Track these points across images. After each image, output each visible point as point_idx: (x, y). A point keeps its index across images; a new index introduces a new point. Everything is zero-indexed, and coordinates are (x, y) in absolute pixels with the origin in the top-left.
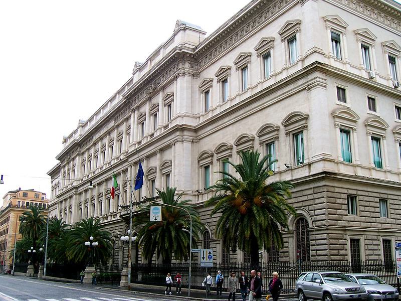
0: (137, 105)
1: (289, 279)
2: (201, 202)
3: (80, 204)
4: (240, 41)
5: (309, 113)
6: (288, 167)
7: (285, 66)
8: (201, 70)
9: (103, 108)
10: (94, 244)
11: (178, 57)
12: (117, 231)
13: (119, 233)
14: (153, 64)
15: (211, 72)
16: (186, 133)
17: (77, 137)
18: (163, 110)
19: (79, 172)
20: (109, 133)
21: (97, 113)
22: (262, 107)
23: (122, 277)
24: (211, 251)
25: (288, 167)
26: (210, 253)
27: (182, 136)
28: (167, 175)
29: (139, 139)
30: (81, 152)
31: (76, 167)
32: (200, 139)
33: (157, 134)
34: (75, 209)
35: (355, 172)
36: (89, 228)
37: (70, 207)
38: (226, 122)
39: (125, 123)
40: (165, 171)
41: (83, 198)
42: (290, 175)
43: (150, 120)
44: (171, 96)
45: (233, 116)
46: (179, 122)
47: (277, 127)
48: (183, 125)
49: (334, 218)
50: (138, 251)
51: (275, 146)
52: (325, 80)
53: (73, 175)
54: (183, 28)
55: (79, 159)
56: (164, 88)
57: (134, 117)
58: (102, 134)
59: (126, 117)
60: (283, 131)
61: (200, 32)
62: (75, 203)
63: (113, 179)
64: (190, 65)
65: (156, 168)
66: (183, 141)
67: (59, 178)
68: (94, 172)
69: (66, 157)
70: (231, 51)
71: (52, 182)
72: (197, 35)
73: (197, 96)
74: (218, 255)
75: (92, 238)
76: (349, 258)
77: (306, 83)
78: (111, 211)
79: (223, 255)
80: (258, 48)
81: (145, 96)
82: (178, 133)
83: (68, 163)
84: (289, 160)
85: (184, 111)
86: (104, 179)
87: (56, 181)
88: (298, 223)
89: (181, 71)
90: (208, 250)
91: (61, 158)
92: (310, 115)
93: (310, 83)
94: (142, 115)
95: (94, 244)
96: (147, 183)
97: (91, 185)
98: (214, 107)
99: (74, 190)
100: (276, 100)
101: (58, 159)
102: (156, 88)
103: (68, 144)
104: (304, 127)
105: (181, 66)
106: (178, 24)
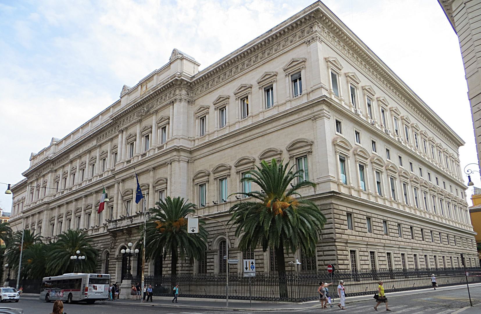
0: (125, 126)
2: (207, 214)
3: (52, 219)
5: (313, 140)
6: (215, 203)
7: (289, 98)
8: (196, 97)
9: (82, 128)
10: (80, 257)
11: (176, 83)
12: (99, 245)
13: (102, 247)
15: (208, 100)
16: (182, 154)
17: (50, 154)
19: (50, 188)
20: (89, 151)
22: (214, 151)
24: (254, 261)
25: (215, 203)
26: (252, 263)
27: (179, 156)
29: (128, 158)
30: (55, 169)
34: (46, 224)
35: (350, 192)
37: (40, 222)
38: (224, 146)
39: (69, 165)
41: (56, 213)
42: (216, 209)
43: (99, 162)
45: (232, 140)
46: (177, 143)
47: (281, 151)
48: (180, 146)
49: (339, 232)
51: (307, 162)
52: (329, 112)
53: (63, 183)
54: (177, 57)
55: (51, 176)
56: (157, 112)
57: (122, 138)
58: (81, 152)
59: (111, 137)
60: (233, 171)
61: (195, 63)
62: (46, 218)
64: (186, 93)
65: (92, 205)
66: (179, 161)
67: (26, 193)
68: (36, 203)
70: (230, 82)
72: (192, 65)
73: (192, 121)
74: (215, 265)
75: (78, 252)
76: (350, 267)
77: (311, 114)
78: (92, 224)
79: (220, 265)
80: (260, 81)
81: (136, 118)
82: (175, 153)
83: (37, 180)
84: (216, 198)
85: (180, 133)
86: (84, 195)
87: (20, 197)
88: (221, 244)
89: (178, 97)
90: (251, 261)
91: (27, 175)
92: (315, 142)
93: (316, 114)
95: (80, 257)
96: (154, 194)
98: (210, 132)
100: (279, 128)
101: (24, 176)
102: (148, 111)
103: (36, 161)
104: (309, 152)
105: (177, 92)
106: (174, 52)
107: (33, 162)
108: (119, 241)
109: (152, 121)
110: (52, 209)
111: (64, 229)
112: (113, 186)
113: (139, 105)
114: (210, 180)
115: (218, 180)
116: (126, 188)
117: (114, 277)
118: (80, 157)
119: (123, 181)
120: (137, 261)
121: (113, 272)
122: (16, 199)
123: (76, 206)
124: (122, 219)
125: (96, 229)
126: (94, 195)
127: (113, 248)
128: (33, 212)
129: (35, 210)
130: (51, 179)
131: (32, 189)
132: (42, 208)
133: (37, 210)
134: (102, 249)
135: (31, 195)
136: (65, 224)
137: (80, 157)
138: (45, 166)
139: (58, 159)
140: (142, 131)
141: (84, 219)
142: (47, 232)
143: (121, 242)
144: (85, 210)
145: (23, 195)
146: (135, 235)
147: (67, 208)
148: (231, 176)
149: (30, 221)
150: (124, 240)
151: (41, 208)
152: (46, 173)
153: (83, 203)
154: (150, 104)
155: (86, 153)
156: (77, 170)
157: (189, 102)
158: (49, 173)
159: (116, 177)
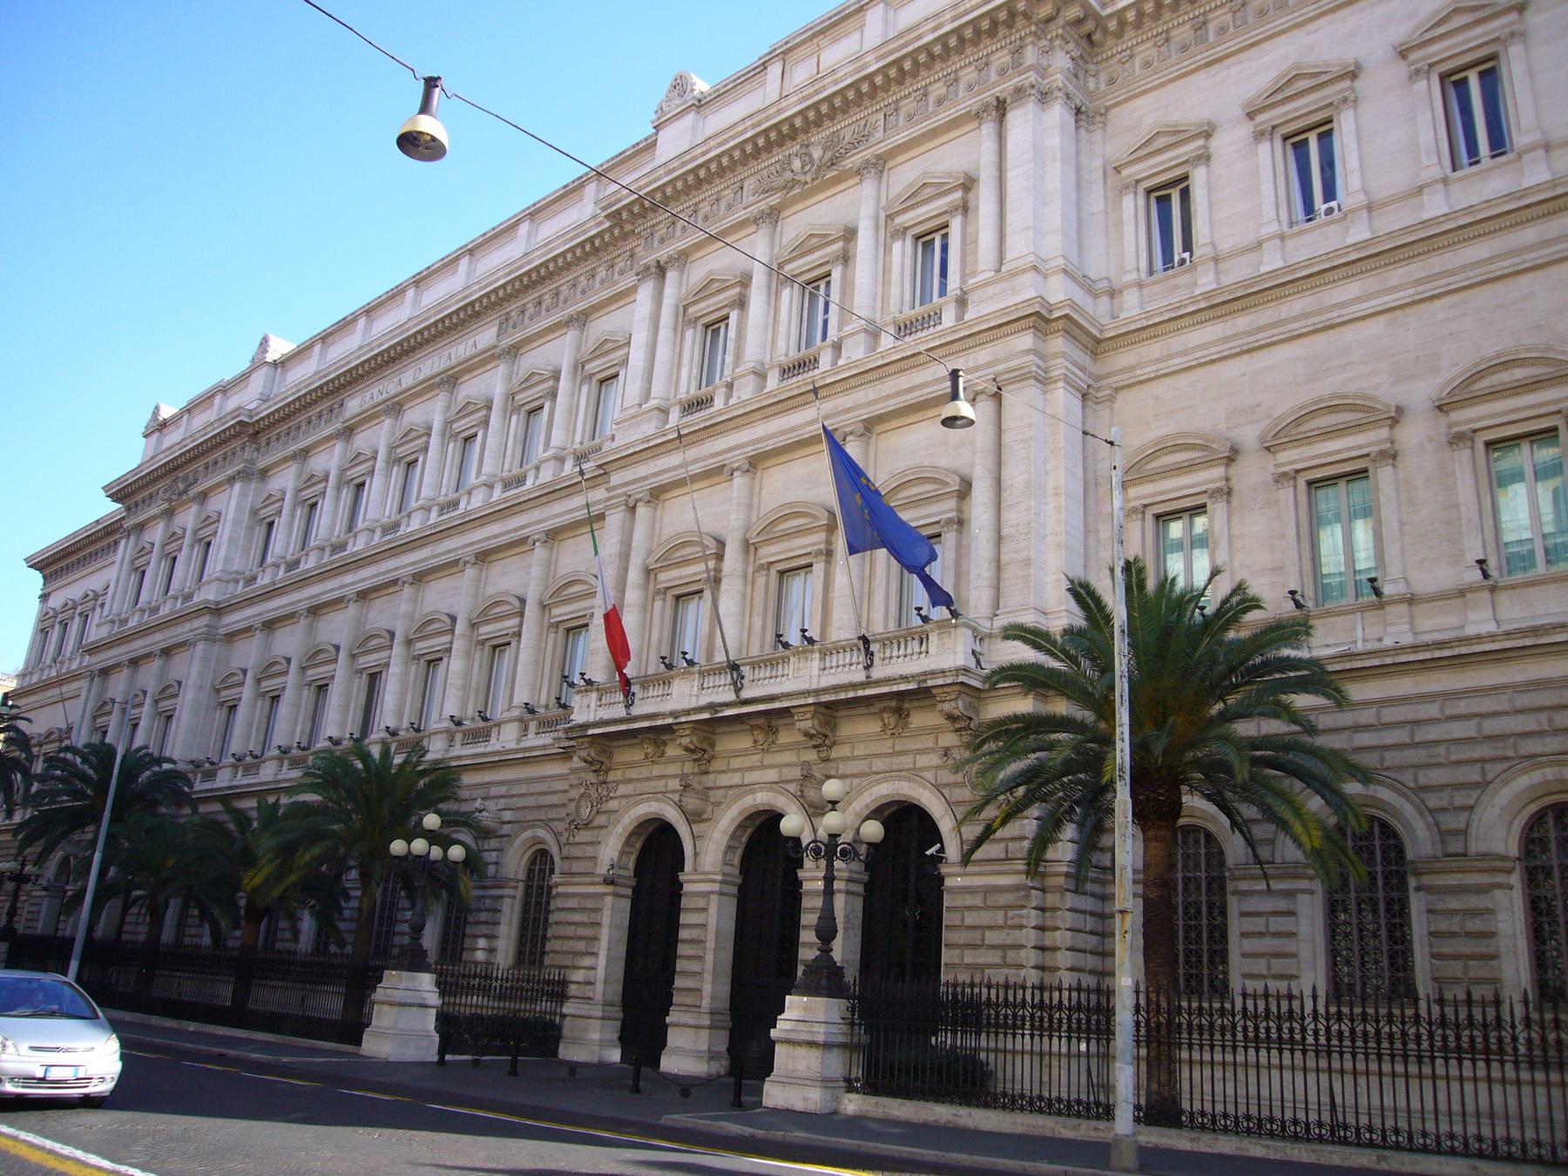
0: (681, 245)
4: (1282, 22)
14: (802, 73)
17: (248, 400)
21: (331, 334)
23: (778, 1048)
28: (320, 687)
30: (261, 465)
32: (1117, 390)
33: (309, 563)
37: (169, 691)
40: (268, 685)
44: (619, 347)
45: (1416, 269)
55: (243, 495)
56: (879, 165)
63: (540, 551)
67: (108, 575)
74: (1305, 954)
78: (236, 746)
83: (169, 513)
88: (533, 862)
91: (122, 492)
99: (205, 620)
103: (173, 437)
107: (159, 442)
108: (622, 789)
112: (595, 520)
113: (782, 135)
114: (1234, 483)
115: (1301, 484)
116: (490, 590)
122: (56, 602)
123: (549, 565)
126: (407, 590)
127: (587, 826)
128: (138, 646)
130: (239, 507)
132: (182, 631)
133: (159, 639)
134: (506, 829)
135: (134, 578)
136: (297, 706)
137: (395, 407)
138: (218, 454)
143: (637, 798)
144: (259, 681)
145: (94, 582)
147: (311, 630)
148: (1408, 462)
151: (179, 630)
152: (219, 485)
153: (404, 608)
154: (845, 127)
155: (431, 388)
157: (1078, 111)
158: (231, 480)
159: (616, 479)
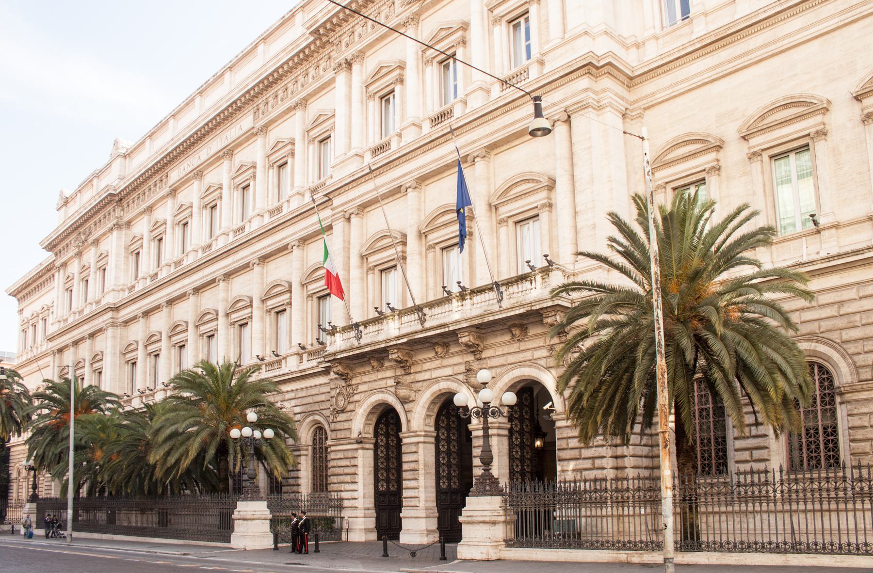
1: (780, 516)
13: (298, 410)
16: (606, 82)
18: (231, 197)
20: (229, 152)
28: (209, 337)
30: (126, 219)
31: (112, 261)
32: (645, 109)
36: (217, 392)
37: (97, 358)
40: (151, 348)
41: (137, 332)
50: (483, 446)
62: (114, 347)
67: (52, 295)
69: (75, 236)
71: (21, 311)
78: (139, 385)
82: (584, 82)
83: (79, 254)
86: (223, 272)
94: (136, 239)
96: (364, 280)
97: (538, 113)
109: (293, 127)
110: (126, 323)
111: (190, 361)
117: (355, 495)
118: (198, 173)
119: (364, 207)
120: (433, 447)
121: (348, 478)
122: (27, 314)
124: (380, 318)
125: (271, 364)
127: (343, 411)
128: (76, 334)
129: (81, 330)
131: (69, 279)
132: (98, 323)
136: (169, 359)
137: (198, 173)
139: (134, 189)
140: (310, 127)
141: (228, 340)
142: (136, 378)
146: (427, 366)
149: (69, 358)
150: (391, 382)
151: (96, 322)
152: (104, 234)
155: (219, 158)
156: (195, 210)
159: (336, 202)
